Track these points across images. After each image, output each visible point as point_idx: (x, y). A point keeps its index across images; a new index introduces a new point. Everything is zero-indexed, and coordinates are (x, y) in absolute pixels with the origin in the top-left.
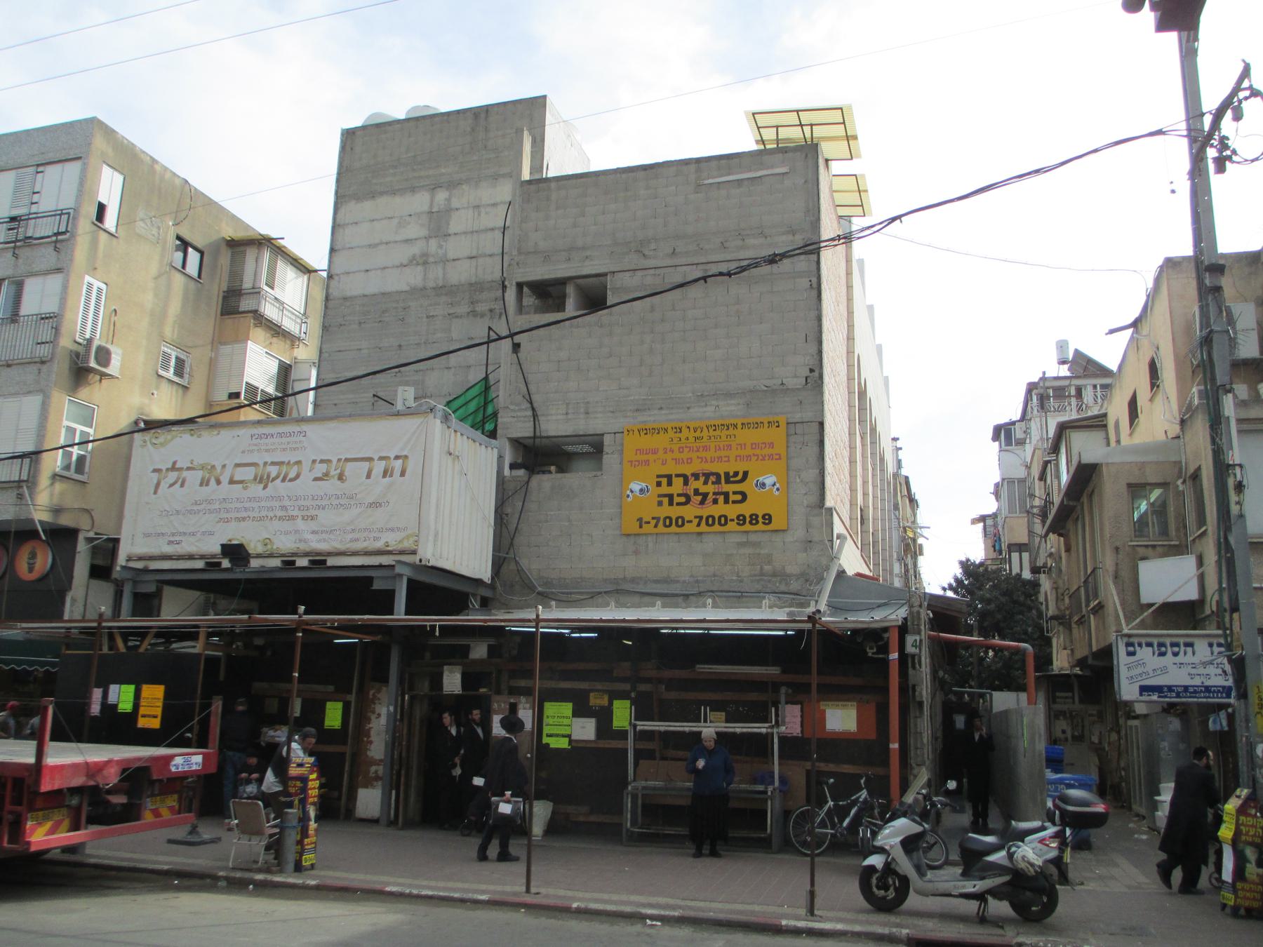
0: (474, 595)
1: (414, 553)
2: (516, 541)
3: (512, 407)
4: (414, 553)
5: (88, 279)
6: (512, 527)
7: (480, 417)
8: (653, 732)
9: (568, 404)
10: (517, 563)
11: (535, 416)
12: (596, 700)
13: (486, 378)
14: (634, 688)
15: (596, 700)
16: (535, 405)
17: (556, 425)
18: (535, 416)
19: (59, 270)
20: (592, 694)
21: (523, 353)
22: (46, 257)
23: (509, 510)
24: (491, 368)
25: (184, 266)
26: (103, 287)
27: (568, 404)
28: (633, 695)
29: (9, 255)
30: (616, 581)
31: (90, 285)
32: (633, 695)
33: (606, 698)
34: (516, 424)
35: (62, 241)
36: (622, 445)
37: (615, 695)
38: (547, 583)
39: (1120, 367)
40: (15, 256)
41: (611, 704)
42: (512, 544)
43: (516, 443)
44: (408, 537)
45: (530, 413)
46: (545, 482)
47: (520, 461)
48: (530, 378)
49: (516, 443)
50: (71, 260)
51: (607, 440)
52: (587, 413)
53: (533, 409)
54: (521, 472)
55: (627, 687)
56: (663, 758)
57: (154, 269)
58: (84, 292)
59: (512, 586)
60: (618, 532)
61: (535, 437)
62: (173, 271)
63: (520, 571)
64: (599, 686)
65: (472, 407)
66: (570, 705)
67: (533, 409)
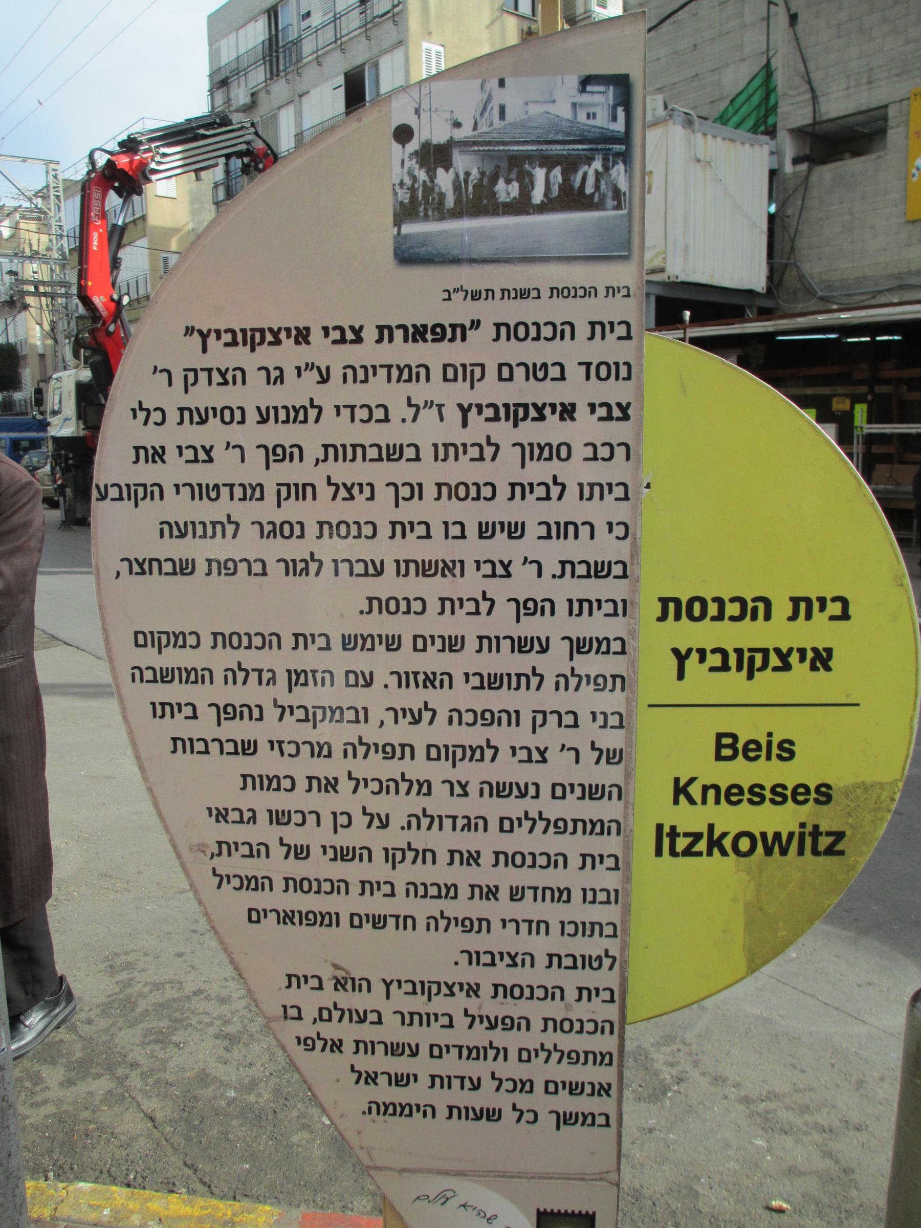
0: (750, 307)
1: (662, 270)
2: (798, 245)
3: (791, 93)
4: (662, 270)
5: (425, 45)
6: (792, 232)
7: (763, 112)
8: (892, 435)
9: (849, 77)
10: (797, 267)
11: (814, 98)
12: (840, 405)
13: (768, 65)
14: (871, 391)
15: (840, 405)
16: (815, 85)
17: (838, 104)
18: (814, 98)
19: (400, 43)
20: (834, 400)
21: (799, 27)
22: (387, 33)
23: (790, 212)
24: (771, 54)
25: (516, 8)
26: (441, 49)
27: (849, 77)
28: (870, 398)
29: (363, 38)
30: (899, 276)
31: (428, 51)
32: (870, 398)
33: (848, 402)
34: (794, 112)
35: (398, 13)
36: (908, 114)
37: (856, 399)
38: (829, 287)
39: (254, 19)
40: (368, 38)
41: (852, 408)
42: (792, 248)
43: (799, 133)
44: (657, 256)
45: (808, 96)
46: (826, 173)
47: (808, 152)
48: (809, 53)
49: (799, 133)
50: (407, 31)
51: (892, 111)
52: (870, 83)
53: (812, 90)
54: (804, 167)
55: (863, 389)
56: (902, 462)
57: (486, 18)
58: (424, 59)
59: (795, 293)
60: (903, 220)
61: (815, 123)
62: (505, 16)
63: (801, 277)
64: (840, 390)
65: (755, 100)
66: (814, 411)
67: (812, 90)
